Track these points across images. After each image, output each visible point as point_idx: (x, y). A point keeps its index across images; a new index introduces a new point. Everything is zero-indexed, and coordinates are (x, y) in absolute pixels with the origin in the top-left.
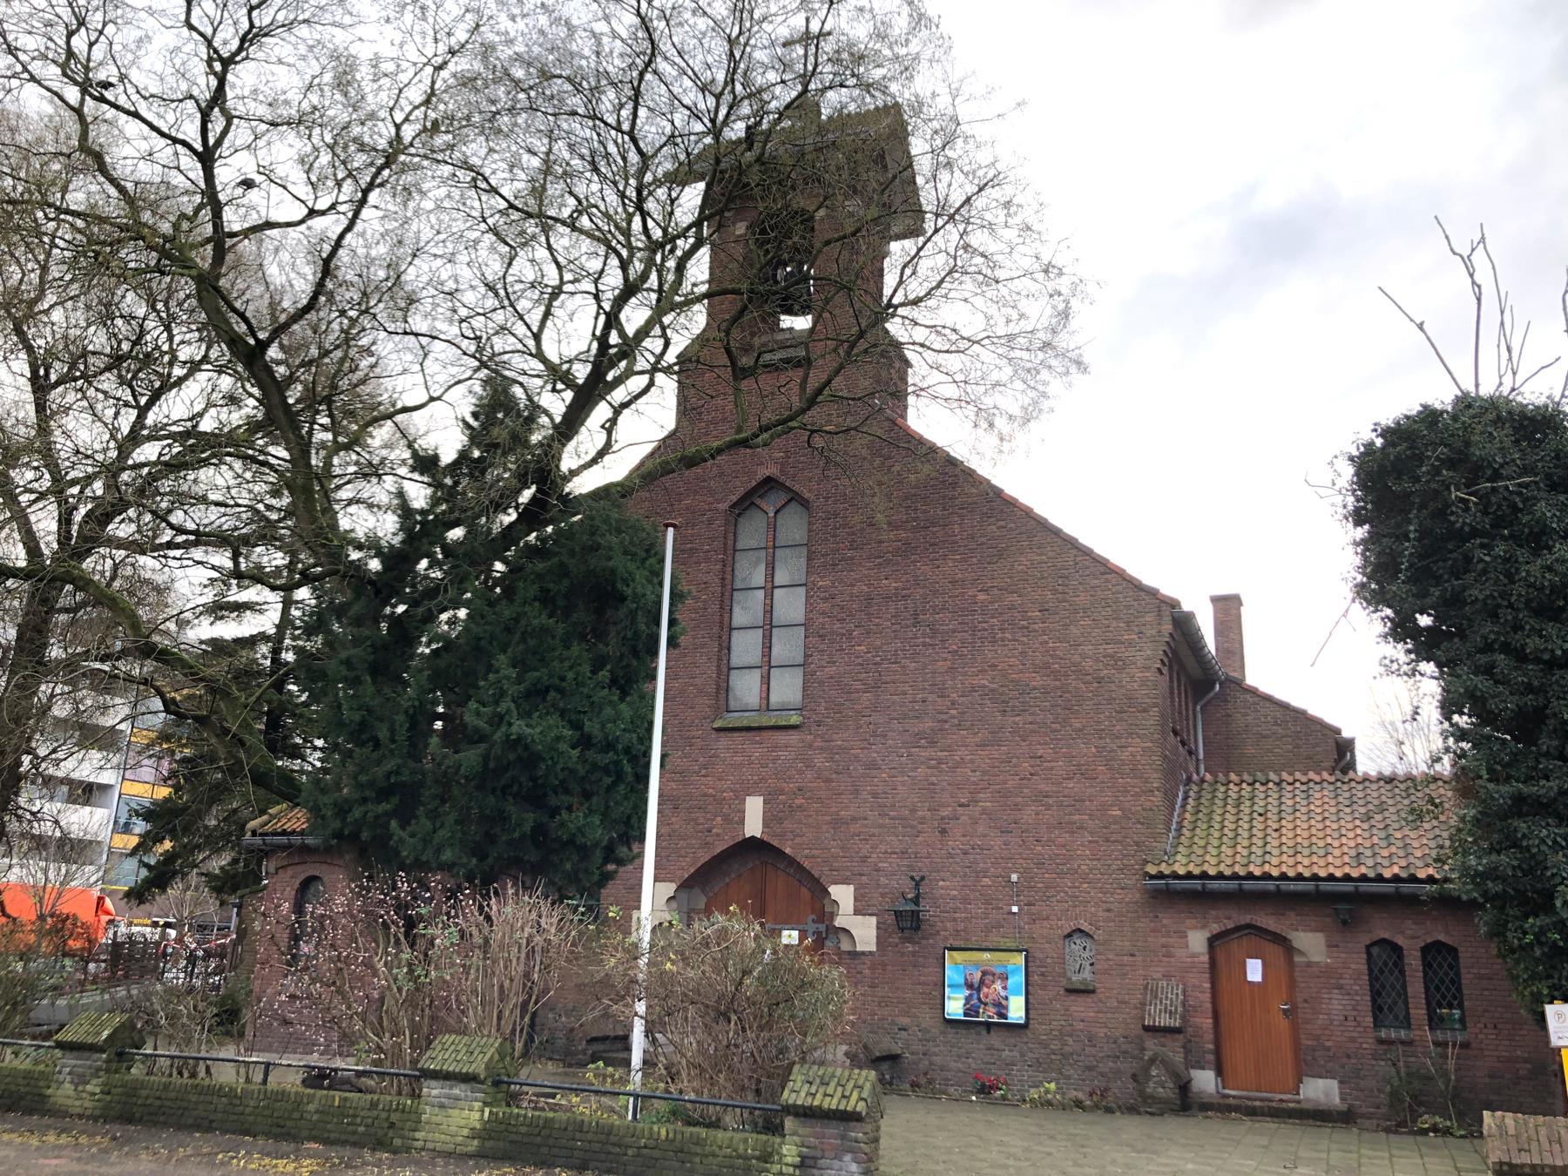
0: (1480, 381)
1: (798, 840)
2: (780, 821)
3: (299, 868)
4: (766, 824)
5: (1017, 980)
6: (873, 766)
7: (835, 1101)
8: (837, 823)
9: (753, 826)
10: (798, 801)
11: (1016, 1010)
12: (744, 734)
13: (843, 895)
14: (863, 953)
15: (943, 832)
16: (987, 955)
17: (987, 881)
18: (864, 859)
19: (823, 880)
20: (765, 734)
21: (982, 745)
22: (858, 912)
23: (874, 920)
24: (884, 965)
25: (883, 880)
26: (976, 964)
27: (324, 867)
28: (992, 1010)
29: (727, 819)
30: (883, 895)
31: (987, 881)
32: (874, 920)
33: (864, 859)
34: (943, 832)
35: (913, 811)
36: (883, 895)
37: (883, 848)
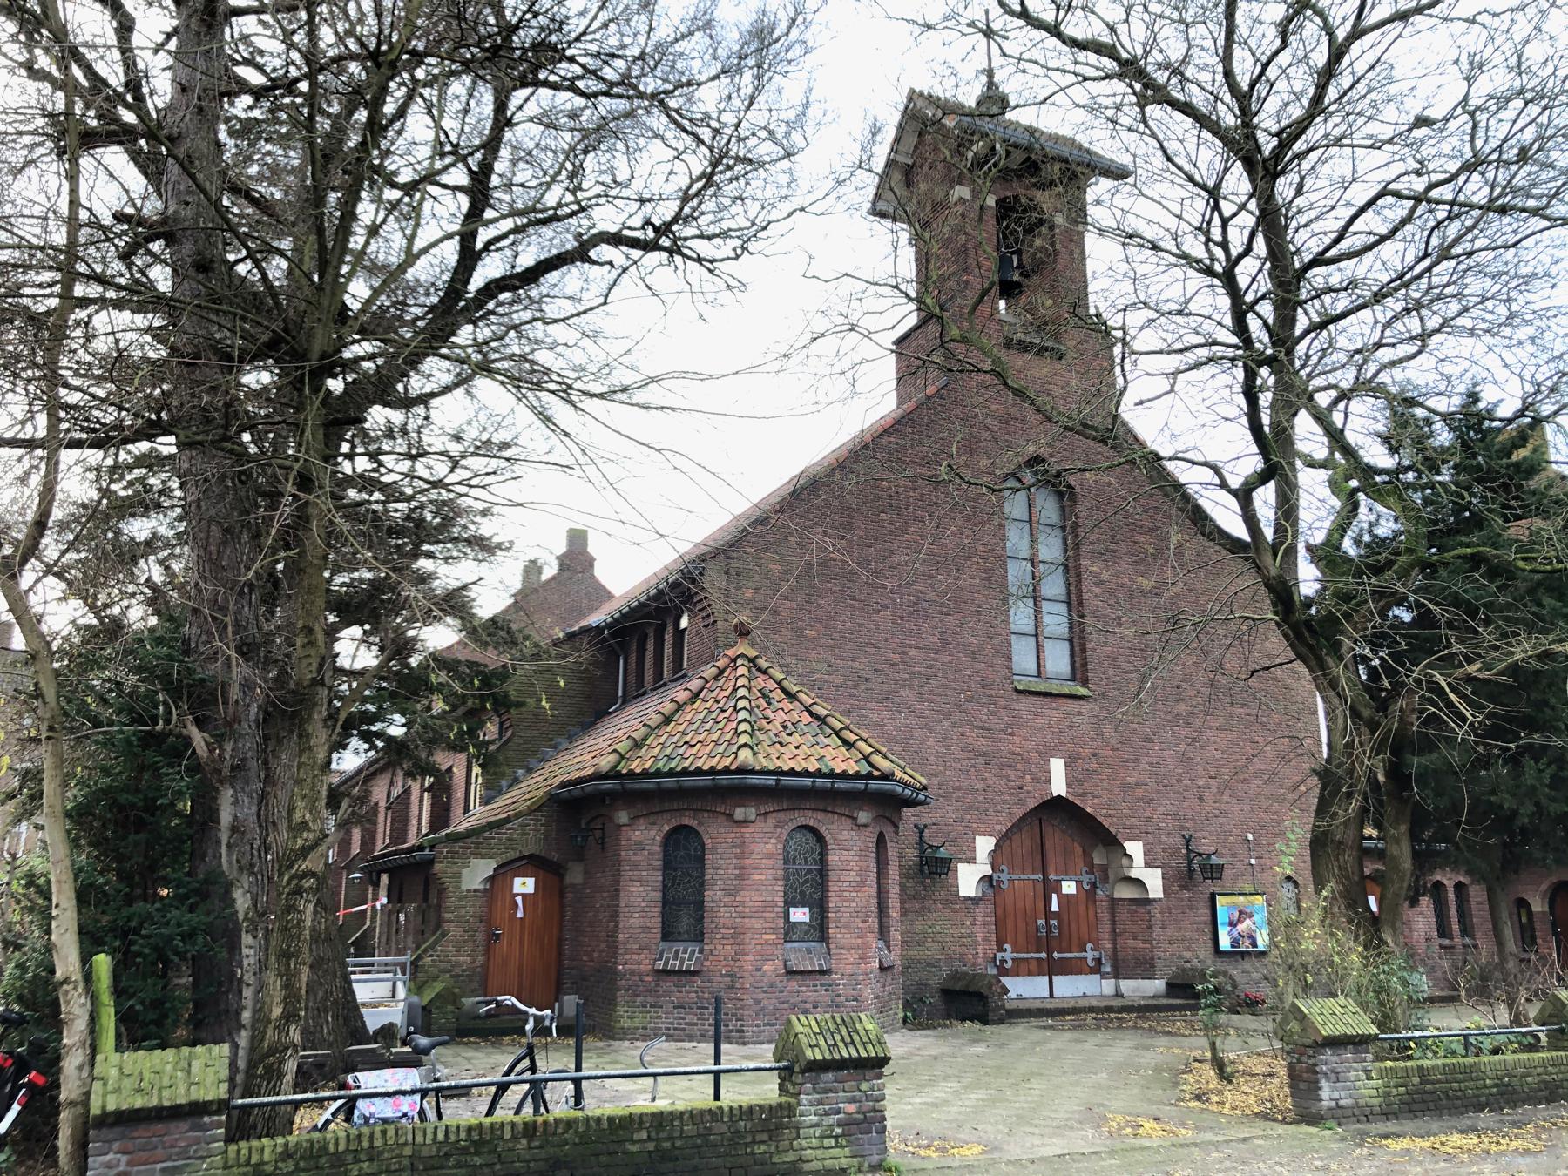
0: (677, 414)
1: (1096, 801)
2: (1081, 783)
3: (789, 815)
4: (1069, 785)
5: (1260, 917)
6: (1147, 739)
7: (182, 1089)
8: (1125, 786)
9: (1059, 787)
10: (1094, 766)
11: (1262, 941)
12: (1047, 700)
13: (1135, 848)
14: (1154, 900)
15: (1201, 798)
16: (1241, 898)
17: (1232, 840)
18: (1148, 820)
19: (1119, 837)
20: (1061, 701)
21: (1221, 729)
22: (1148, 865)
23: (1159, 871)
24: (1169, 909)
25: (1164, 838)
26: (1234, 905)
27: (820, 816)
28: (1247, 942)
29: (1035, 779)
30: (1164, 850)
31: (1232, 840)
32: (1159, 871)
33: (1148, 820)
34: (1201, 798)
35: (1179, 781)
36: (1164, 850)
37: (1161, 810)
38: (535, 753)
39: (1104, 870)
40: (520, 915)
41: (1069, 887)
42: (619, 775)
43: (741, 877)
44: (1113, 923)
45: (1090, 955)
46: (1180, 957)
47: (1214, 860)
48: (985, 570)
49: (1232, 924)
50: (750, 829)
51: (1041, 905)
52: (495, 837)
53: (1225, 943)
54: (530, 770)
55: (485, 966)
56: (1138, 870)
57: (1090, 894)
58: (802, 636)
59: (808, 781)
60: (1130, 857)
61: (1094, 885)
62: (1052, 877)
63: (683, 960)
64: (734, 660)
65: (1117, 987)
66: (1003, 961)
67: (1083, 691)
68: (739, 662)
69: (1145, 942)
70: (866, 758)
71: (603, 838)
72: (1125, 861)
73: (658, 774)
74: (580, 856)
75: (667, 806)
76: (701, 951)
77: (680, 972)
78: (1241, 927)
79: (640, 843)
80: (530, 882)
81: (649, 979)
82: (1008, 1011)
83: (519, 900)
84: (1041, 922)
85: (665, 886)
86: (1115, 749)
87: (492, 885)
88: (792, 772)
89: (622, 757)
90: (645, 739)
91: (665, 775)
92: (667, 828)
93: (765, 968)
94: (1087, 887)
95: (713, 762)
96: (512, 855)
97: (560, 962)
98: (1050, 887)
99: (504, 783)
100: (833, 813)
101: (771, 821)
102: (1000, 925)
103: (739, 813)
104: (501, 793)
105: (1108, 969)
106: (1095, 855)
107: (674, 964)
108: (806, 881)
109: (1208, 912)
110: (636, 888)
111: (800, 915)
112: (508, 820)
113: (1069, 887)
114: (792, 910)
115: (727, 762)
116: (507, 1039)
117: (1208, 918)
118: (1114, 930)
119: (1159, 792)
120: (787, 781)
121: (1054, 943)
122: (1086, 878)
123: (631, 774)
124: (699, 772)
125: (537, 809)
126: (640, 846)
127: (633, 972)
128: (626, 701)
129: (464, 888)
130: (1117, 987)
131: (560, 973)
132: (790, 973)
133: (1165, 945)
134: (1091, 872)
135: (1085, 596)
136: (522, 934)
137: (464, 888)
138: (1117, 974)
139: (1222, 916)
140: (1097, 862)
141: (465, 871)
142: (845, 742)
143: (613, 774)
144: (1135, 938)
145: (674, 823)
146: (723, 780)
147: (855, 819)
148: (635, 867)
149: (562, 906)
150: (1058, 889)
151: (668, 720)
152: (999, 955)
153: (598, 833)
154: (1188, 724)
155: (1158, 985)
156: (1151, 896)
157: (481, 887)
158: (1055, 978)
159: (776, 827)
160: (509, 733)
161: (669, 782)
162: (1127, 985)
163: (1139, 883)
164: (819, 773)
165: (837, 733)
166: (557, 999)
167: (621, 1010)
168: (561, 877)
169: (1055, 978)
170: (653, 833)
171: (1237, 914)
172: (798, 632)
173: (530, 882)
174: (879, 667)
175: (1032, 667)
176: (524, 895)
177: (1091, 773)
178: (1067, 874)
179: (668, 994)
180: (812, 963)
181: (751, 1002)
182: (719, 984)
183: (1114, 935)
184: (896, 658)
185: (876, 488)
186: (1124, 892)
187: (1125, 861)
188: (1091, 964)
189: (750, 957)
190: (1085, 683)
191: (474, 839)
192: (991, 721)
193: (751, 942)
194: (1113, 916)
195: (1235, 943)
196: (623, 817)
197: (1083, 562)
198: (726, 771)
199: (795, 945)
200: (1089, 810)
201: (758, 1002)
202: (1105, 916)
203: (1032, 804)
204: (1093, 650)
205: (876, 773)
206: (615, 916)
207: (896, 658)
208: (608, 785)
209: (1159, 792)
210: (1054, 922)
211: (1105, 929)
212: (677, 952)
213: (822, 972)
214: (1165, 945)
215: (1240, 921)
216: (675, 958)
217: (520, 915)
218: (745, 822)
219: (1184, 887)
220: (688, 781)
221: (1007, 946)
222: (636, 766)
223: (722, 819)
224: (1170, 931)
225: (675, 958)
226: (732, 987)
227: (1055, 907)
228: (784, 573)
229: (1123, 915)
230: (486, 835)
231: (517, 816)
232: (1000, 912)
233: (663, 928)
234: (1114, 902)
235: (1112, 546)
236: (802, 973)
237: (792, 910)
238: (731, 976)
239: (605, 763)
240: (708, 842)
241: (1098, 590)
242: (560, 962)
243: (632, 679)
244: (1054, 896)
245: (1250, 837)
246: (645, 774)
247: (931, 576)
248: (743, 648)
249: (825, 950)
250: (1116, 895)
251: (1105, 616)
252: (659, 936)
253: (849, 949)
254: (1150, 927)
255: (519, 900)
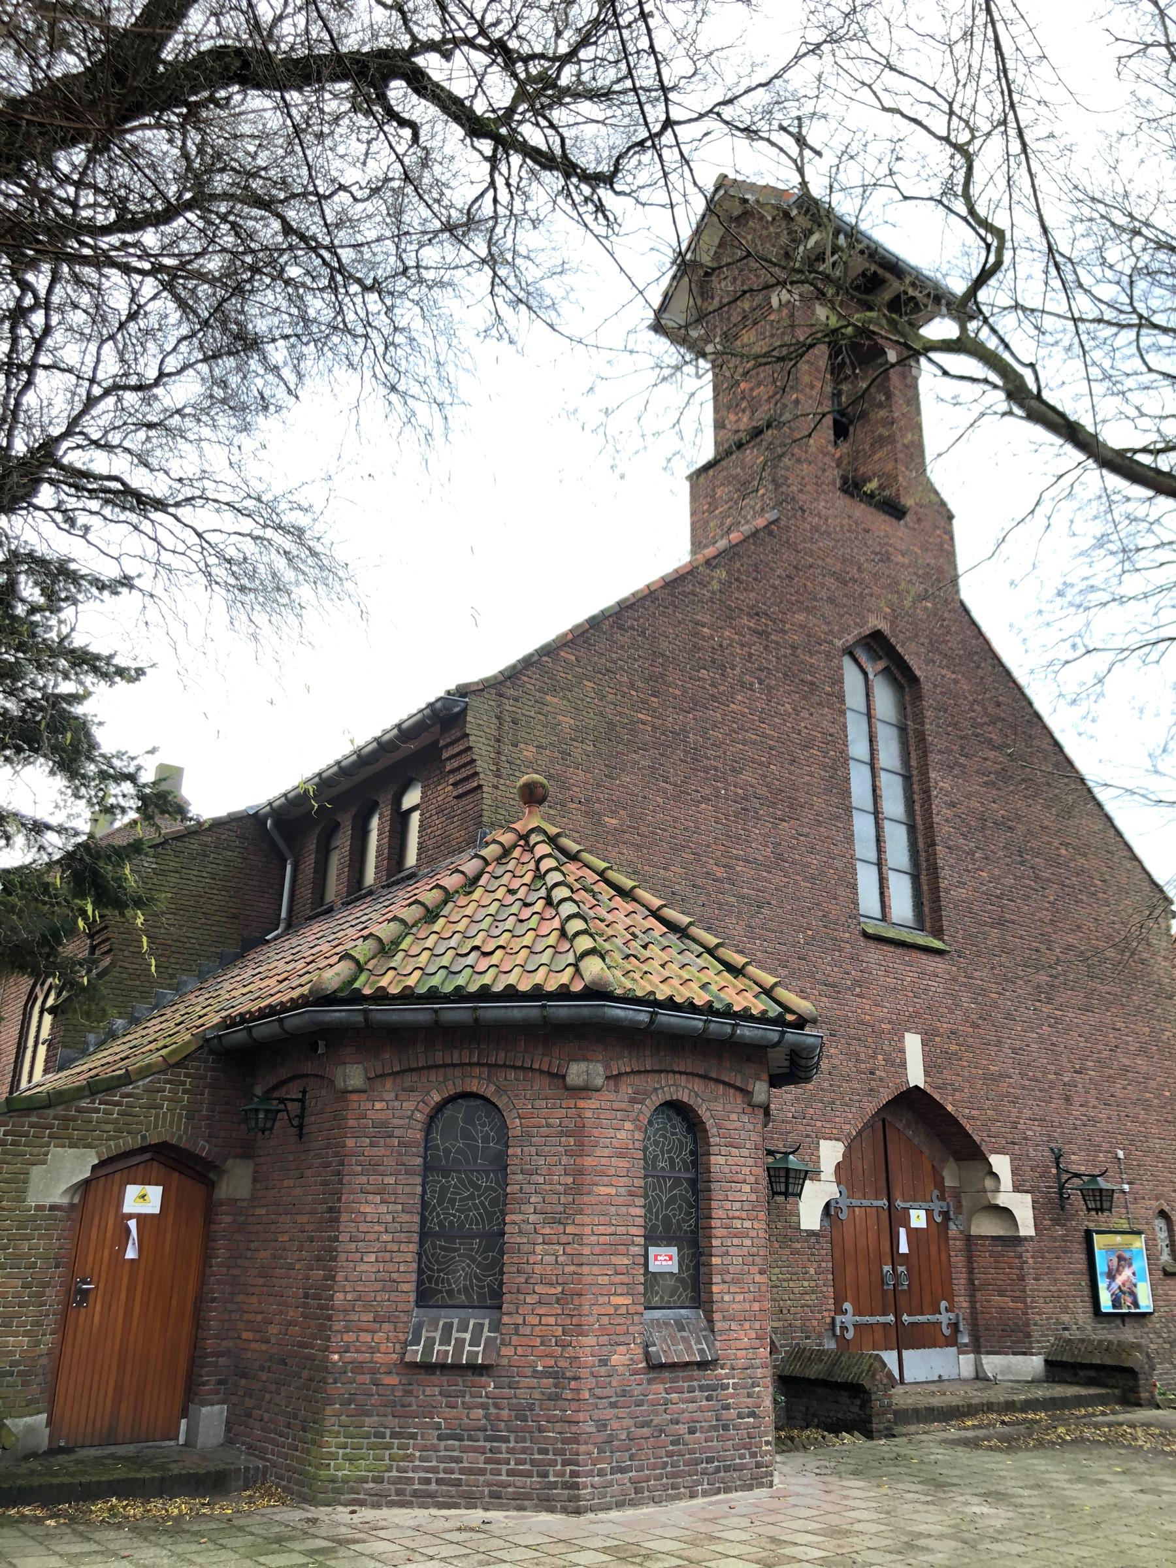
3: (651, 1082)
4: (927, 1073)
5: (1141, 1264)
9: (916, 1076)
10: (954, 1047)
11: (1146, 1302)
12: (899, 951)
13: (1001, 1164)
14: (1026, 1239)
15: (1068, 1099)
18: (1015, 1125)
20: (916, 955)
22: (1017, 1189)
23: (1028, 1197)
25: (1032, 1153)
27: (698, 1085)
34: (1068, 1099)
35: (1044, 1074)
37: (1027, 1113)
38: (145, 995)
39: (957, 1194)
40: (131, 1253)
41: (918, 1219)
42: (357, 997)
43: (577, 1189)
44: (971, 1271)
45: (944, 1318)
46: (1058, 1322)
47: (1102, 1183)
48: (824, 767)
49: (1111, 1276)
50: (593, 1103)
51: (886, 1244)
52: (99, 1109)
53: (1106, 1304)
54: (135, 1021)
55: (57, 1356)
56: (1007, 1197)
57: (939, 1227)
58: (599, 823)
59: (697, 1023)
60: (996, 1176)
61: (946, 1215)
62: (899, 1203)
63: (460, 1343)
64: (525, 837)
65: (978, 1366)
66: (844, 1328)
67: (937, 944)
68: (534, 838)
69: (1015, 1299)
70: (768, 992)
71: (301, 1116)
72: (989, 1183)
73: (433, 995)
74: (247, 1151)
75: (439, 1057)
76: (496, 1327)
77: (456, 1368)
78: (1119, 1280)
79: (384, 1124)
80: (155, 1193)
81: (392, 1380)
82: (895, 1413)
83: (132, 1224)
84: (887, 1268)
85: (424, 1205)
86: (975, 1026)
87: (84, 1198)
88: (670, 1004)
89: (360, 968)
90: (396, 942)
91: (446, 998)
92: (437, 1098)
93: (615, 1359)
94: (939, 1219)
95: (538, 978)
96: (129, 1142)
97: (196, 1343)
98: (896, 1218)
99: (91, 1038)
100: (718, 1081)
101: (627, 1089)
102: (838, 1273)
103: (576, 1072)
104: (85, 1053)
105: (966, 1340)
106: (945, 1173)
107: (443, 1351)
108: (671, 1201)
109: (1083, 1257)
110: (371, 1207)
111: (665, 1259)
112: (127, 1079)
113: (918, 1219)
114: (653, 1251)
115: (565, 978)
116: (98, 1508)
117: (1083, 1266)
118: (971, 1282)
119: (1023, 1087)
120: (667, 1018)
121: (903, 1301)
122: (937, 1206)
123: (381, 996)
124: (511, 993)
125: (177, 1063)
126: (383, 1130)
127: (359, 1368)
128: (293, 925)
129: (32, 1201)
130: (978, 1366)
131: (196, 1358)
132: (655, 1367)
133: (1040, 1303)
134: (942, 1198)
135: (936, 819)
136: (131, 1290)
137: (32, 1201)
138: (977, 1348)
139: (1101, 1266)
140: (948, 1183)
141: (36, 1170)
142: (730, 968)
143: (348, 996)
144: (1002, 1293)
145: (451, 1090)
146: (562, 1010)
147: (746, 1093)
148: (373, 1167)
149: (208, 1239)
150: (906, 1222)
151: (431, 915)
152: (839, 1319)
153: (294, 1108)
154: (1050, 1000)
155: (1034, 1364)
156: (1023, 1232)
157: (64, 1201)
158: (906, 1354)
159: (632, 1101)
160: (107, 962)
161: (457, 1013)
162: (993, 1363)
163: (1006, 1213)
164: (709, 1009)
165: (710, 951)
166: (184, 1414)
167: (332, 1443)
168: (211, 1185)
169: (906, 1354)
170: (409, 1105)
171: (1115, 1261)
172: (594, 817)
173: (155, 1193)
174: (699, 882)
175: (876, 911)
176: (141, 1218)
177: (949, 1056)
178: (916, 1198)
179: (429, 1410)
180: (689, 1349)
181: (590, 1427)
182: (529, 1389)
183: (972, 1289)
184: (720, 873)
185: (695, 634)
186: (985, 1227)
187: (989, 1183)
188: (947, 1332)
189: (590, 1340)
190: (938, 933)
191: (60, 1110)
192: (835, 974)
193: (593, 1311)
194: (970, 1260)
195: (1116, 1302)
196: (353, 1075)
197: (933, 775)
198: (564, 993)
199: (657, 1314)
200: (950, 1108)
201: (602, 1425)
202: (958, 1260)
203: (885, 1096)
204: (947, 891)
205: (790, 1017)
206: (327, 1257)
207: (720, 873)
208: (337, 1014)
209: (1023, 1087)
210: (901, 1269)
211: (960, 1281)
212: (448, 1328)
213: (703, 1365)
214: (1040, 1303)
215: (1119, 1271)
216: (445, 1340)
217: (131, 1253)
218: (585, 1090)
219: (1056, 1221)
220: (492, 1011)
221: (847, 1306)
222: (390, 983)
223: (540, 1084)
224: (1045, 1284)
225: (445, 1340)
226: (556, 1397)
227: (904, 1248)
228: (576, 729)
229: (984, 1260)
230: (83, 1104)
231: (145, 1071)
232: (838, 1254)
233: (420, 1283)
234: (969, 1239)
235: (962, 760)
236: (673, 1366)
237: (653, 1251)
238: (556, 1375)
239: (333, 976)
240: (515, 1125)
241: (949, 813)
242: (196, 1343)
243: (306, 892)
244: (902, 1231)
245: (1121, 1154)
246: (407, 996)
247: (761, 764)
248: (531, 820)
249: (703, 1324)
250: (974, 1231)
251: (958, 848)
252: (413, 1297)
253: (740, 1321)
254: (1022, 1278)
255: (132, 1224)
